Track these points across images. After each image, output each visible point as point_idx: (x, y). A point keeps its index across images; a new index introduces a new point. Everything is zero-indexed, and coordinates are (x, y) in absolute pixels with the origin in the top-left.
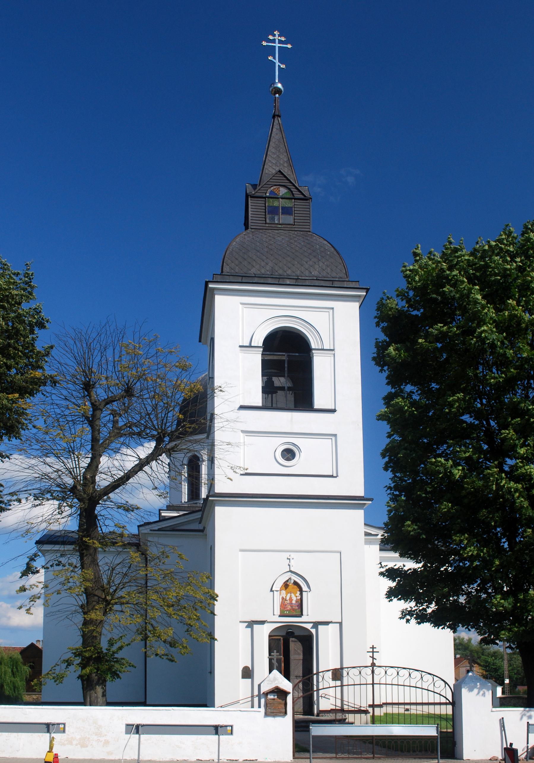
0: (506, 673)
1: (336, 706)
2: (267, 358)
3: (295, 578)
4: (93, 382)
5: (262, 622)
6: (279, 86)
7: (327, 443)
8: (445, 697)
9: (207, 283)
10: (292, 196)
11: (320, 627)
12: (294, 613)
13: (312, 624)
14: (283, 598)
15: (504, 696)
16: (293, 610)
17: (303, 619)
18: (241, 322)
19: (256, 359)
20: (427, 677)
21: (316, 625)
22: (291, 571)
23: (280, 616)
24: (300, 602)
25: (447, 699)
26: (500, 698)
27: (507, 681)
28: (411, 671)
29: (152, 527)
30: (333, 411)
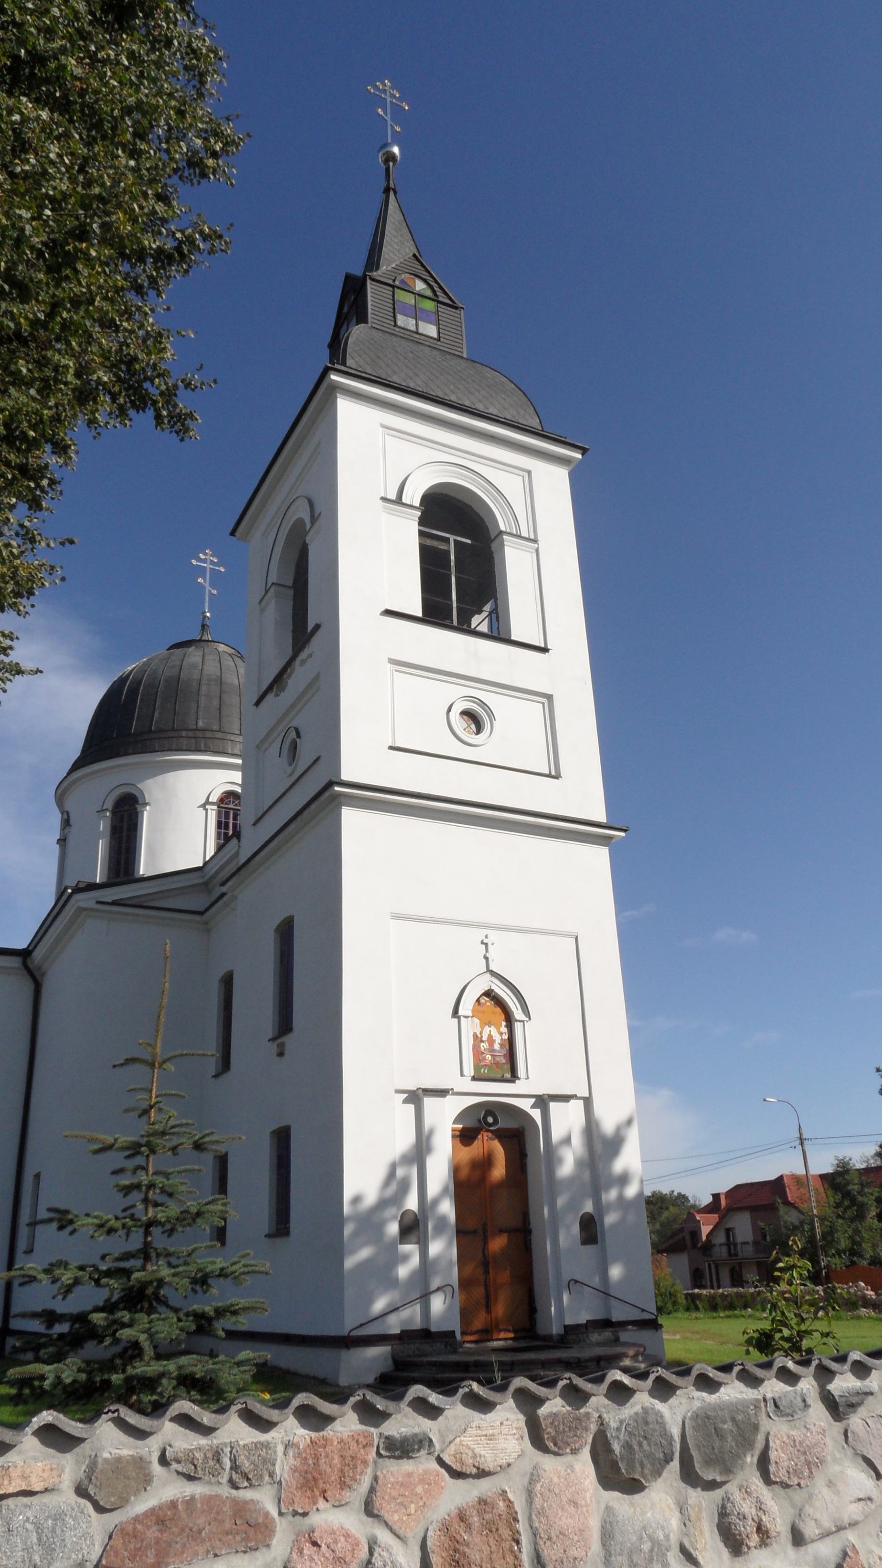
4: (67, 278)
5: (442, 1093)
11: (553, 1106)
13: (533, 1100)
16: (497, 1064)
18: (382, 459)
21: (542, 1102)
23: (474, 1079)
24: (507, 1047)
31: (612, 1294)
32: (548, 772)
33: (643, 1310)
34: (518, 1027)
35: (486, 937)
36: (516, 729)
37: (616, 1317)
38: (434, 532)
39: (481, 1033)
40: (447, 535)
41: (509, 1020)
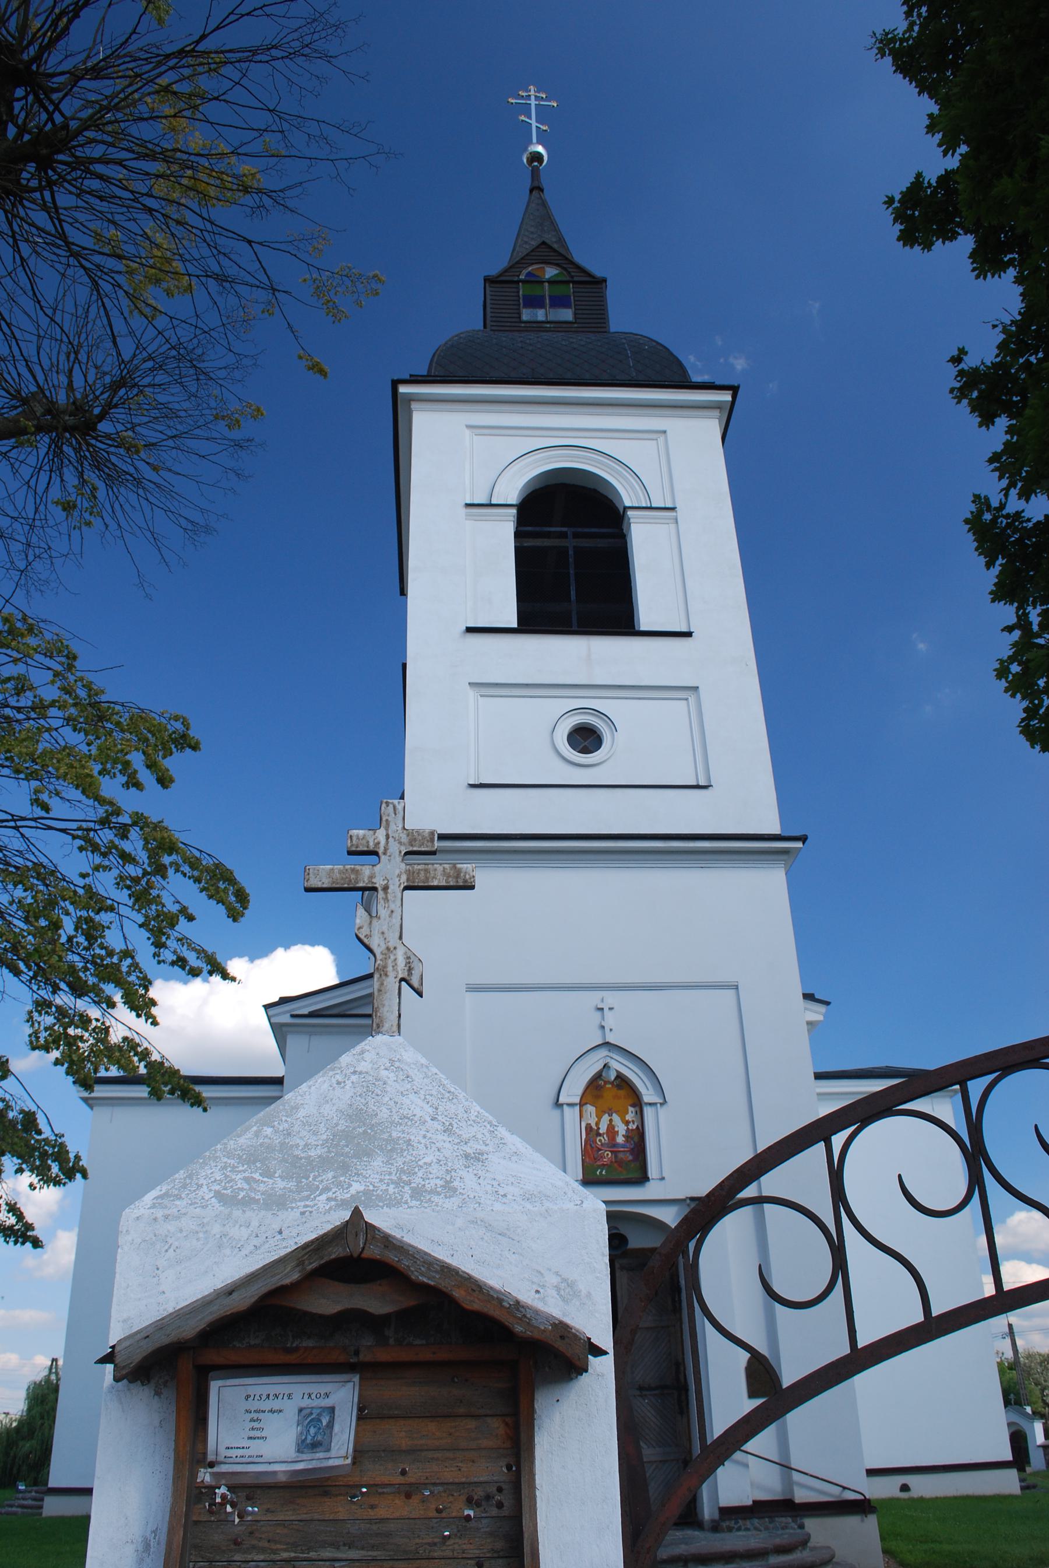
2: (529, 543)
3: (619, 1065)
6: (540, 149)
7: (677, 709)
9: (395, 383)
10: (568, 278)
12: (624, 1176)
14: (589, 1128)
16: (620, 1163)
17: (650, 1191)
18: (469, 462)
19: (502, 533)
22: (607, 1044)
24: (636, 1139)
29: (294, 1010)
30: (688, 634)
31: (793, 1466)
32: (695, 783)
33: (844, 1488)
34: (648, 1112)
35: (602, 1000)
36: (640, 739)
37: (801, 1496)
38: (586, 530)
39: (597, 1124)
40: (564, 529)
41: (638, 1103)
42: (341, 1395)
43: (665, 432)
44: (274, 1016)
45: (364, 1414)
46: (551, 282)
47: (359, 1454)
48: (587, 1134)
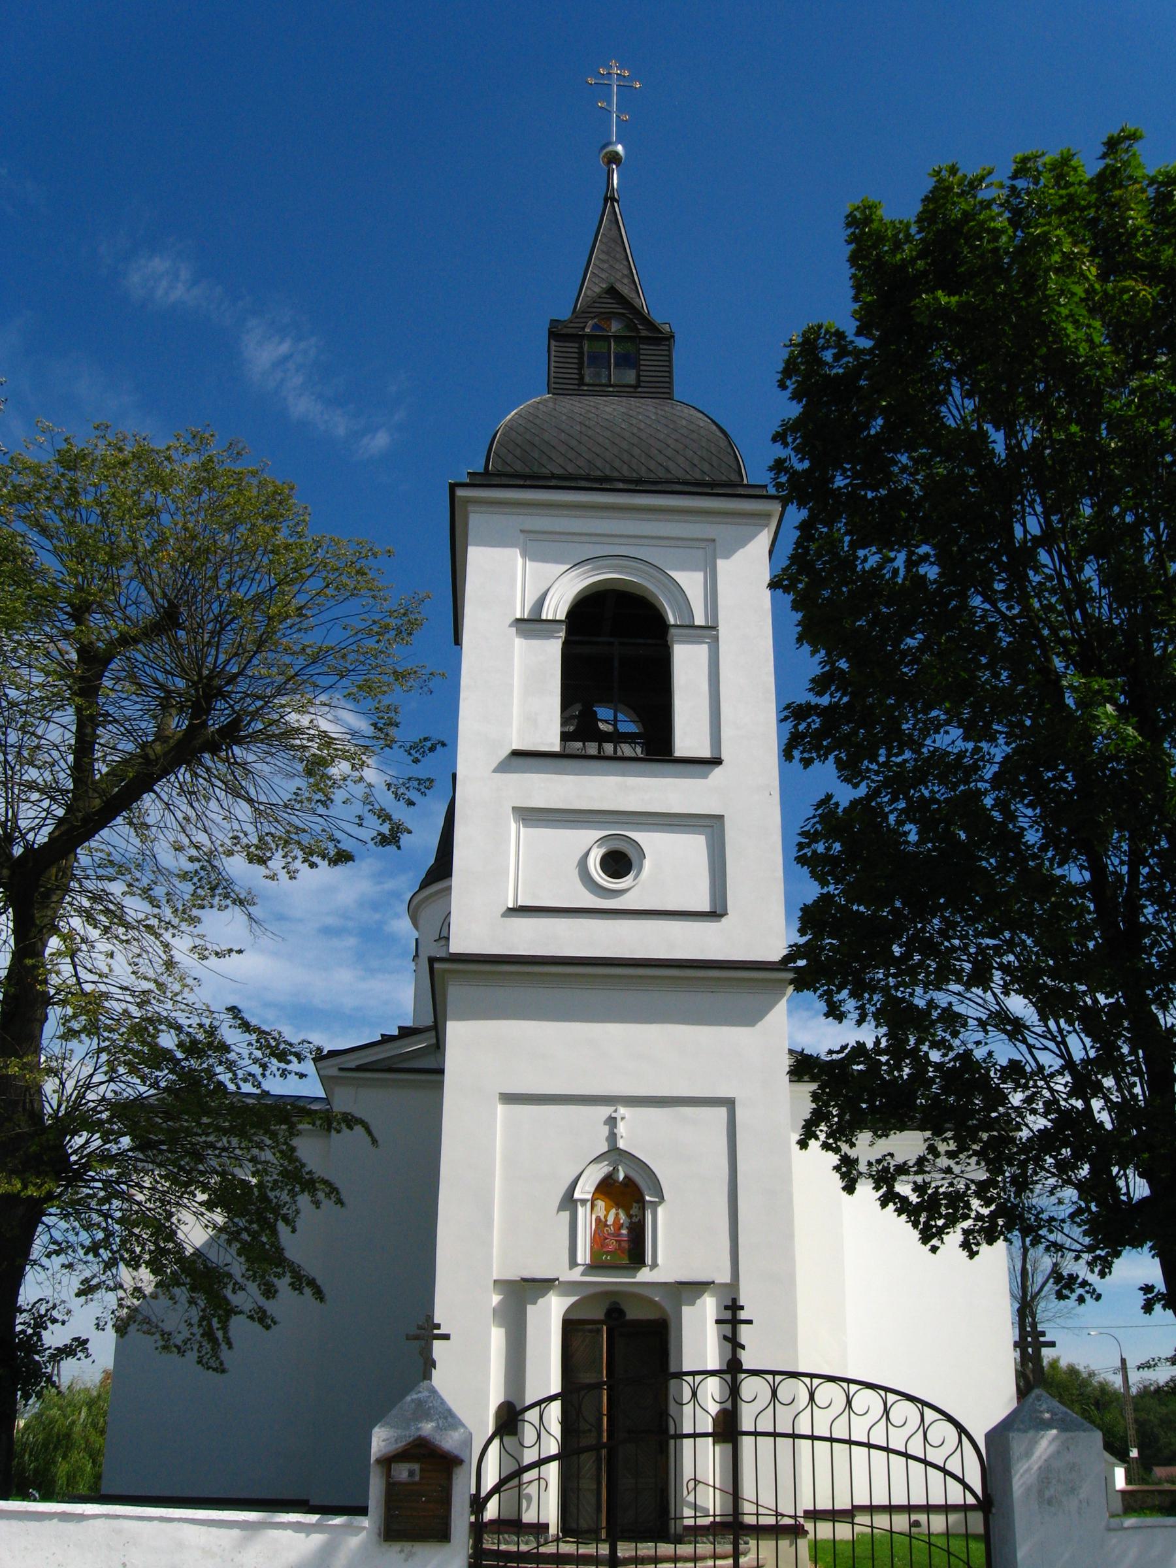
0: (1131, 1432)
1: (872, 1527)
8: (961, 1481)
14: (598, 1219)
15: (1130, 1488)
17: (644, 1275)
19: (549, 653)
20: (903, 1411)
25: (966, 1487)
26: (1123, 1492)
27: (1134, 1453)
28: (853, 1388)
39: (606, 1217)
40: (612, 640)
41: (641, 1201)
42: (416, 1467)
43: (714, 540)
44: (324, 1068)
45: (422, 1470)
46: (618, 339)
47: (421, 1478)
48: (597, 1225)
